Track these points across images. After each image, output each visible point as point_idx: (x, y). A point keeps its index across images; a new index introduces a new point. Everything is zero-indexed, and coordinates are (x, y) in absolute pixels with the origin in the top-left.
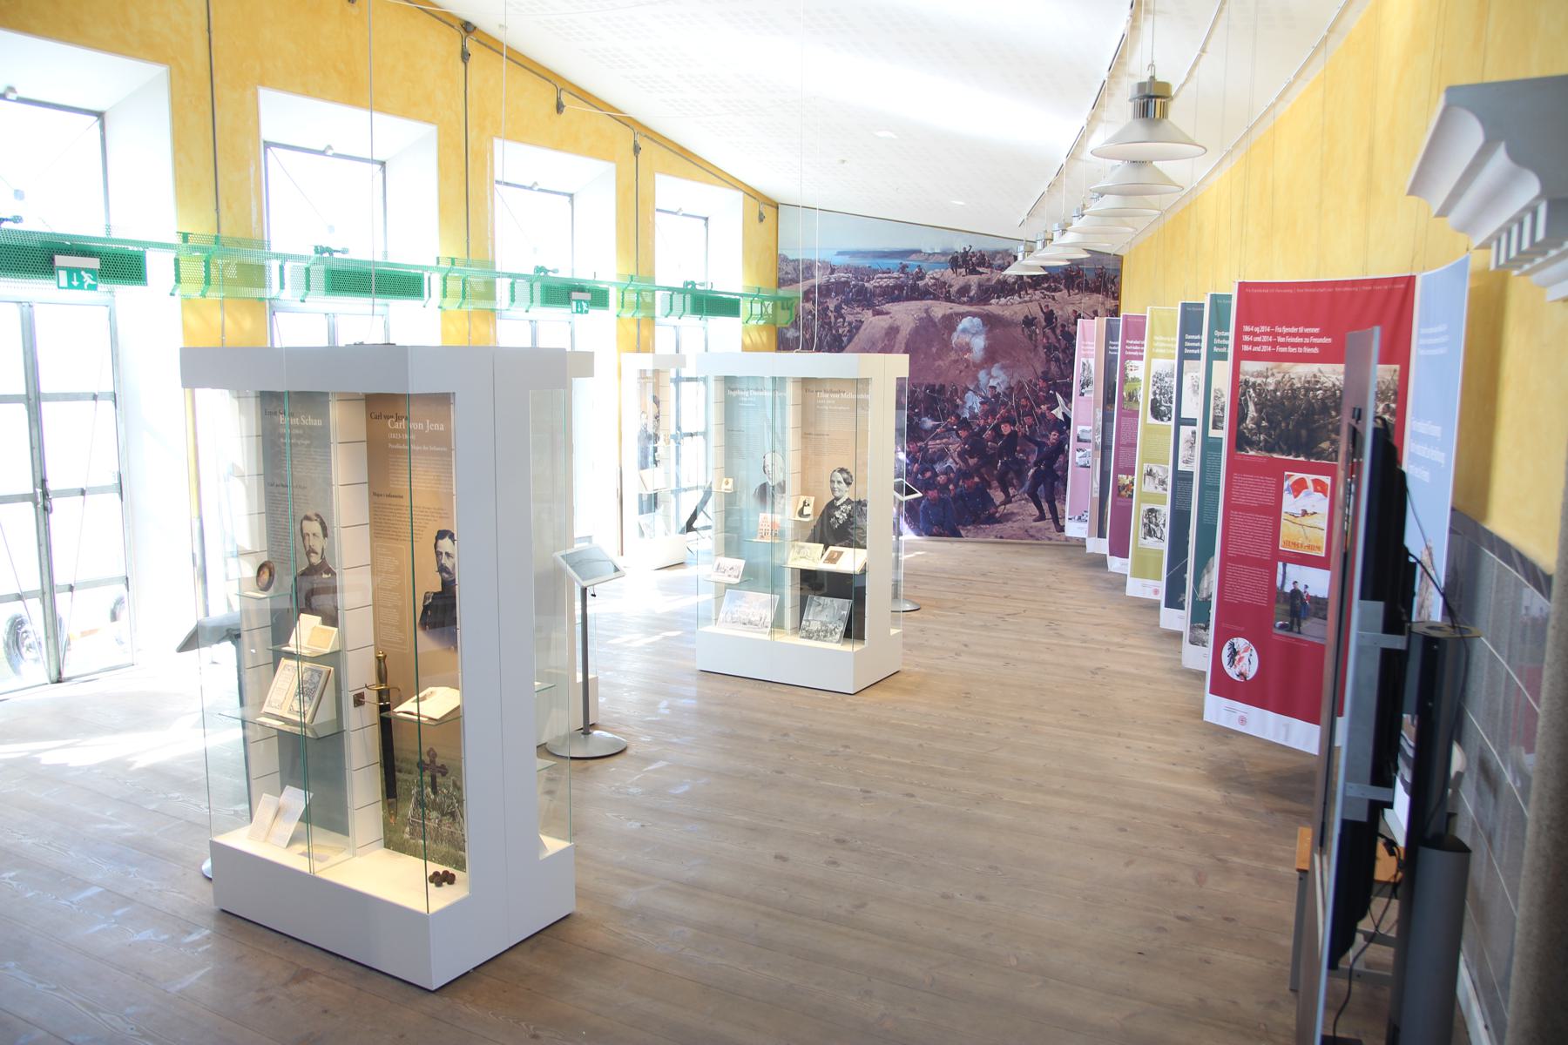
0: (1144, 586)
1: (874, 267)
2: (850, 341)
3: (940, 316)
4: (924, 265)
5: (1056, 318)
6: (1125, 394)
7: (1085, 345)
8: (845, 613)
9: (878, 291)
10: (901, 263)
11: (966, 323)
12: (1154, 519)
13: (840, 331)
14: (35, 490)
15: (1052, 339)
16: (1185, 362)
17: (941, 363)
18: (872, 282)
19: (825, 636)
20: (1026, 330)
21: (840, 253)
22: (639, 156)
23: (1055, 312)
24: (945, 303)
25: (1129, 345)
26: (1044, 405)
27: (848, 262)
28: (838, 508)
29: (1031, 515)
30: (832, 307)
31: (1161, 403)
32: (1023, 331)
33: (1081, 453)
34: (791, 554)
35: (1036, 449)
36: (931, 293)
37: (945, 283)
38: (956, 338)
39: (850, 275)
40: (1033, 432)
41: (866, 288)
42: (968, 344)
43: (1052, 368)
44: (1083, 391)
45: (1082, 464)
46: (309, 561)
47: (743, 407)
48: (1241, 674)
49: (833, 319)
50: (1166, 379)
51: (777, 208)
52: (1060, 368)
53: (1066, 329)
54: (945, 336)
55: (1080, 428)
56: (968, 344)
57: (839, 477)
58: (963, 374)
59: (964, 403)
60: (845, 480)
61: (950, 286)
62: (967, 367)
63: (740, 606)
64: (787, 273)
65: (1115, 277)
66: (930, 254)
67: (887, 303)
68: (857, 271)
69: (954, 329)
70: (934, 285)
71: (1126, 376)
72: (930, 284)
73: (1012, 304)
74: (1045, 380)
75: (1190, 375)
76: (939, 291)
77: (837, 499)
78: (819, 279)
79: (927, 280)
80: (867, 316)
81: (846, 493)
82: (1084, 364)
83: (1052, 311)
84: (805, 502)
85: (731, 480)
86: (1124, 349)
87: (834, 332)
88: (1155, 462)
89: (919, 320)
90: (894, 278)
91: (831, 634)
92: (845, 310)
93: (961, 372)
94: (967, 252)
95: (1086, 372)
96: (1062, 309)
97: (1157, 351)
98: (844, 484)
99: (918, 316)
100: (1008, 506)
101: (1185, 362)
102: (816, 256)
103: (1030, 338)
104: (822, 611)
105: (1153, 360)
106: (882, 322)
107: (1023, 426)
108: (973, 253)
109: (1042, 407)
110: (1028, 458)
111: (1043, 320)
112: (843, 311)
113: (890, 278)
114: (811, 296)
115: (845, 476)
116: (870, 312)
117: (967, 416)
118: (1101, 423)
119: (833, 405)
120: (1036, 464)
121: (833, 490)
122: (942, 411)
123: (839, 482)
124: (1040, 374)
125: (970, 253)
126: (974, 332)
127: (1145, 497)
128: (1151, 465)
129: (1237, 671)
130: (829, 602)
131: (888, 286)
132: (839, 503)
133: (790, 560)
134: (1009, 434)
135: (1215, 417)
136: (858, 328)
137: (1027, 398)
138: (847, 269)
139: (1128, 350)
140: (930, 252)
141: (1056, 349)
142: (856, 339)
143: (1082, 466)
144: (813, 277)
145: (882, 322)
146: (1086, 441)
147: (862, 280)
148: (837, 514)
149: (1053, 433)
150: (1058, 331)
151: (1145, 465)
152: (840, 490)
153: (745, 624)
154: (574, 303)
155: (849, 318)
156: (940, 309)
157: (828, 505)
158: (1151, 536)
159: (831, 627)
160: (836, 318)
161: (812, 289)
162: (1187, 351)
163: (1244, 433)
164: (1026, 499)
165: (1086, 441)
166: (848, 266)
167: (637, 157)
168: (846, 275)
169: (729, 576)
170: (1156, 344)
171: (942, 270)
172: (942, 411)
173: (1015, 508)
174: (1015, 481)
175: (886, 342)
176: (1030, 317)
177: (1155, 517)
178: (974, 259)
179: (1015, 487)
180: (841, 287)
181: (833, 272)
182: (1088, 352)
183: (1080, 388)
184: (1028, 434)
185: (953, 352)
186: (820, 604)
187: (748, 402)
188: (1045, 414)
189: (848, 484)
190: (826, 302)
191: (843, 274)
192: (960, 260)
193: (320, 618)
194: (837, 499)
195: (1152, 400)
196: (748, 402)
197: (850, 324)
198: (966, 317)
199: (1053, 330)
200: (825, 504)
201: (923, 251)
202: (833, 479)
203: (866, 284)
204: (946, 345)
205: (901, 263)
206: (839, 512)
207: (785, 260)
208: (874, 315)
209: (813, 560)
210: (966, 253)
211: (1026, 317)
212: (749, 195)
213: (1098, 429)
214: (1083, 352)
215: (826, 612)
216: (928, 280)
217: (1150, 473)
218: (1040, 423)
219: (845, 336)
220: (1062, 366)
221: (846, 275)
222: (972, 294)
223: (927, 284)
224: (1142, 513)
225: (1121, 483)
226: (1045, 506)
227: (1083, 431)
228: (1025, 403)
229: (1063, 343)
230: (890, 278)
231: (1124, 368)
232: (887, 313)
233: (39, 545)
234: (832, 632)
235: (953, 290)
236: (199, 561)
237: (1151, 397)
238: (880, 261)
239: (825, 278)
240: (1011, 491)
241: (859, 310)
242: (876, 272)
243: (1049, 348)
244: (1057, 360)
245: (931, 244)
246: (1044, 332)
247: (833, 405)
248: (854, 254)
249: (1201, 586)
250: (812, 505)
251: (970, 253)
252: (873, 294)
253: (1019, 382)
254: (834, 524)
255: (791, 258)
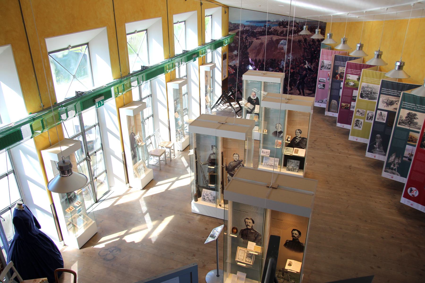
0: (354, 138)
1: (257, 26)
2: (249, 47)
3: (275, 39)
4: (271, 25)
5: (307, 40)
6: (345, 83)
7: (323, 56)
8: (299, 164)
9: (258, 32)
10: (264, 24)
11: (282, 41)
12: (358, 122)
13: (247, 44)
14: (86, 156)
15: (306, 46)
16: (381, 95)
17: (275, 53)
18: (256, 30)
19: (293, 170)
20: (299, 43)
21: (247, 22)
22: (202, 6)
23: (307, 38)
24: (276, 36)
25: (348, 70)
26: (302, 64)
27: (249, 24)
28: (297, 139)
29: (297, 93)
30: (244, 37)
31: (363, 94)
32: (298, 44)
33: (320, 85)
34: (284, 150)
35: (300, 76)
36: (273, 33)
37: (277, 30)
38: (279, 46)
39: (250, 28)
40: (299, 71)
41: (254, 32)
42: (282, 48)
43: (305, 54)
44: (321, 69)
45: (320, 88)
46: (247, 227)
47: (270, 112)
48: (413, 195)
49: (244, 41)
50: (365, 88)
51: (228, 8)
52: (307, 54)
53: (310, 43)
54: (276, 45)
55: (320, 78)
56: (282, 48)
57: (298, 131)
58: (281, 56)
59: (281, 64)
60: (300, 132)
61: (278, 31)
62: (282, 54)
63: (268, 161)
64: (231, 27)
65: (324, 29)
66: (273, 22)
67: (261, 36)
68: (252, 27)
69: (279, 43)
70: (274, 31)
71: (346, 78)
72: (272, 30)
73: (295, 36)
74: (303, 57)
75: (382, 98)
76: (275, 33)
77: (297, 136)
78: (240, 29)
79: (272, 29)
80: (255, 40)
81: (299, 135)
82: (322, 61)
83: (306, 38)
84: (288, 137)
85: (266, 130)
86: (346, 71)
87: (245, 44)
88: (360, 108)
89: (269, 41)
90: (262, 29)
91: (295, 170)
92: (248, 38)
93: (280, 55)
94: (283, 21)
95: (323, 64)
96: (309, 38)
97: (364, 81)
98: (299, 133)
99: (269, 40)
100: (291, 91)
101: (381, 95)
102: (240, 22)
103: (300, 46)
104: (292, 163)
105: (362, 83)
106: (259, 41)
107: (297, 70)
108: (285, 21)
109: (302, 65)
110: (297, 78)
111: (303, 41)
112: (248, 38)
113: (261, 29)
114: (238, 34)
115: (300, 131)
116: (255, 39)
117: (281, 67)
118: (331, 82)
119: (297, 114)
120: (300, 80)
121: (296, 134)
122: (275, 66)
123: (298, 133)
124: (302, 55)
125: (284, 22)
126: (284, 44)
127: (356, 117)
128: (359, 109)
129: (412, 194)
130: (294, 161)
131: (260, 31)
132: (297, 138)
133: (284, 152)
134: (292, 72)
135: (399, 122)
136: (252, 43)
137: (298, 62)
138: (249, 26)
139: (348, 71)
140: (273, 21)
141: (307, 49)
142: (251, 46)
143: (320, 88)
144: (239, 28)
145: (259, 41)
146: (321, 82)
147: (253, 29)
148: (297, 140)
149: (304, 72)
150: (307, 44)
151: (357, 109)
152: (298, 135)
153: (270, 166)
154: (193, 59)
155: (249, 40)
156: (275, 38)
157: (294, 138)
158: (357, 126)
159: (295, 168)
160: (245, 40)
161: (239, 32)
162: (382, 92)
163: (423, 144)
164: (296, 89)
165: (321, 82)
166: (249, 25)
167: (201, 7)
168: (249, 28)
169: (266, 154)
170: (364, 79)
171: (276, 27)
172: (275, 66)
173: (293, 91)
174: (293, 84)
175: (260, 47)
176: (300, 40)
177: (358, 122)
178: (285, 23)
179: (293, 86)
180: (247, 31)
181: (245, 27)
182: (324, 58)
183: (320, 68)
184: (298, 72)
185: (278, 50)
186: (291, 162)
187: (272, 110)
188: (302, 66)
189: (300, 133)
190: (243, 36)
191: (247, 28)
192: (281, 24)
193: (255, 243)
194: (297, 136)
195: (361, 93)
196: (272, 110)
197: (249, 42)
198: (282, 40)
199: (306, 44)
200: (293, 137)
201: (271, 21)
202: (296, 132)
203: (254, 31)
204: (276, 48)
205: (264, 24)
206: (297, 140)
207: (230, 23)
208: (256, 40)
209: (291, 152)
210: (283, 22)
211: (299, 40)
212: (223, 7)
213: (330, 84)
214: (322, 58)
215: (293, 164)
216: (272, 30)
217: (358, 111)
218: (301, 69)
219: (248, 45)
220: (308, 53)
221: (249, 28)
222: (284, 33)
223: (272, 31)
224: (355, 121)
225: (342, 105)
226: (301, 91)
227: (321, 79)
228: (297, 64)
229: (309, 47)
230: (261, 29)
231: (346, 76)
232: (260, 39)
233: (89, 170)
234: (295, 169)
235: (279, 32)
236: (124, 162)
237: (361, 92)
238: (258, 24)
239: (242, 29)
240: (292, 87)
241: (252, 38)
242: (257, 27)
243: (305, 49)
244: (307, 52)
245: (273, 19)
246: (304, 44)
247: (297, 114)
248: (251, 22)
249: (389, 160)
250: (290, 138)
251: (284, 22)
252: (256, 33)
253: (296, 58)
254: (295, 142)
255: (232, 23)
